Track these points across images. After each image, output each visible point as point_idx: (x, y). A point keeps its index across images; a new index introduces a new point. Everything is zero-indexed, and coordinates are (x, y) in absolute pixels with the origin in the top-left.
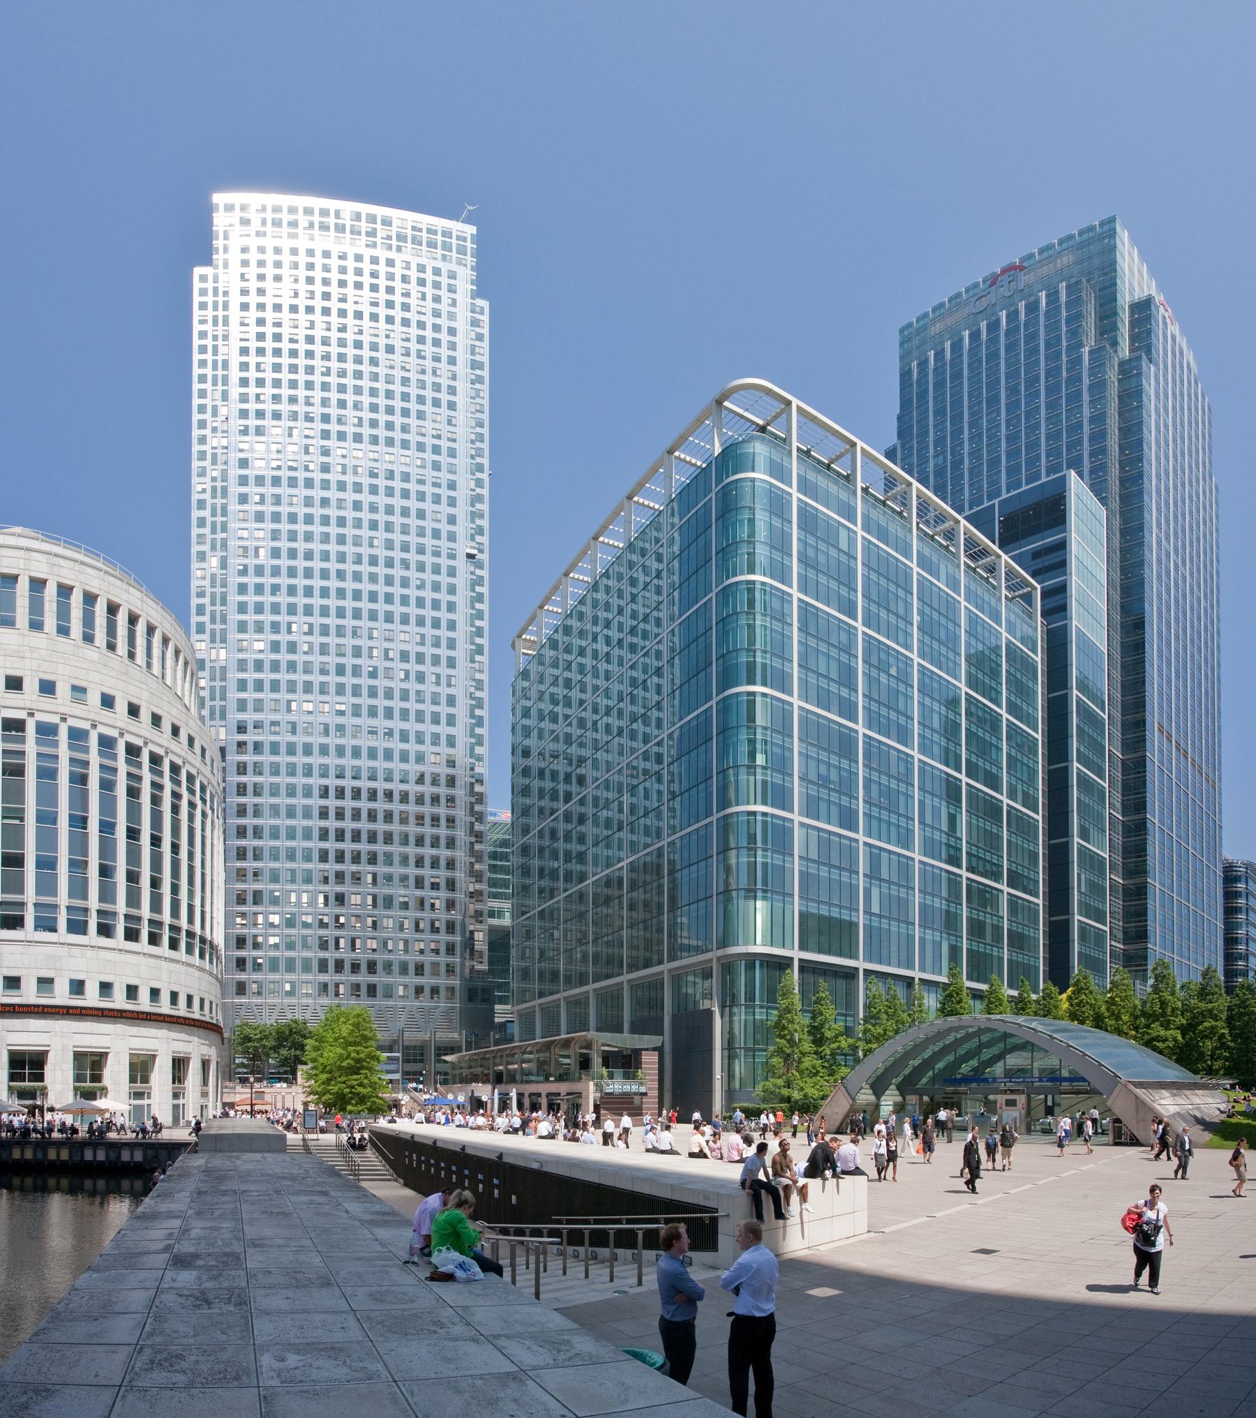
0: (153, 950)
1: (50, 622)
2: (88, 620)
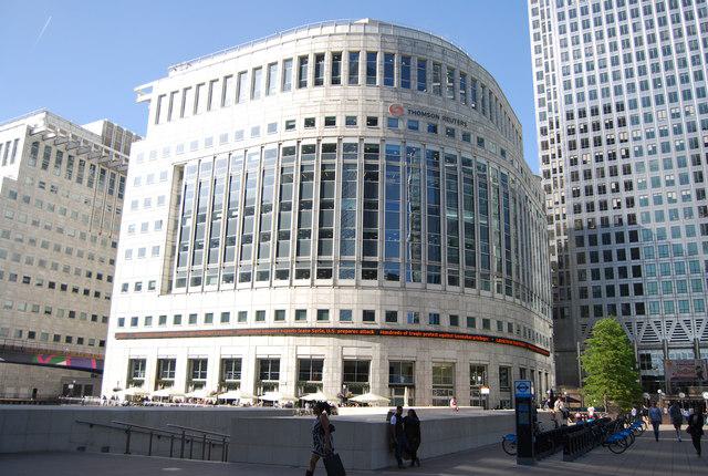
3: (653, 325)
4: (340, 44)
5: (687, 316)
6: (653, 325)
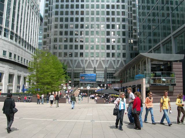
3: (91, 61)
5: (93, 59)
6: (91, 61)
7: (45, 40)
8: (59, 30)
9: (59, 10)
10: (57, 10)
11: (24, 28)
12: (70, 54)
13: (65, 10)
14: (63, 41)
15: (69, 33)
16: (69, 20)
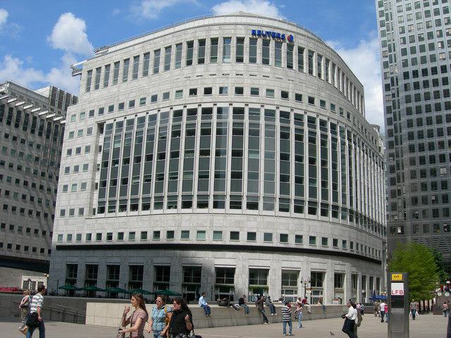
0: (324, 218)
1: (259, 58)
2: (301, 62)
4: (217, 33)
7: (394, 200)
8: (419, 180)
9: (416, 142)
10: (409, 105)
11: (361, 194)
12: (445, 227)
13: (425, 128)
14: (430, 201)
15: (439, 186)
16: (437, 159)
